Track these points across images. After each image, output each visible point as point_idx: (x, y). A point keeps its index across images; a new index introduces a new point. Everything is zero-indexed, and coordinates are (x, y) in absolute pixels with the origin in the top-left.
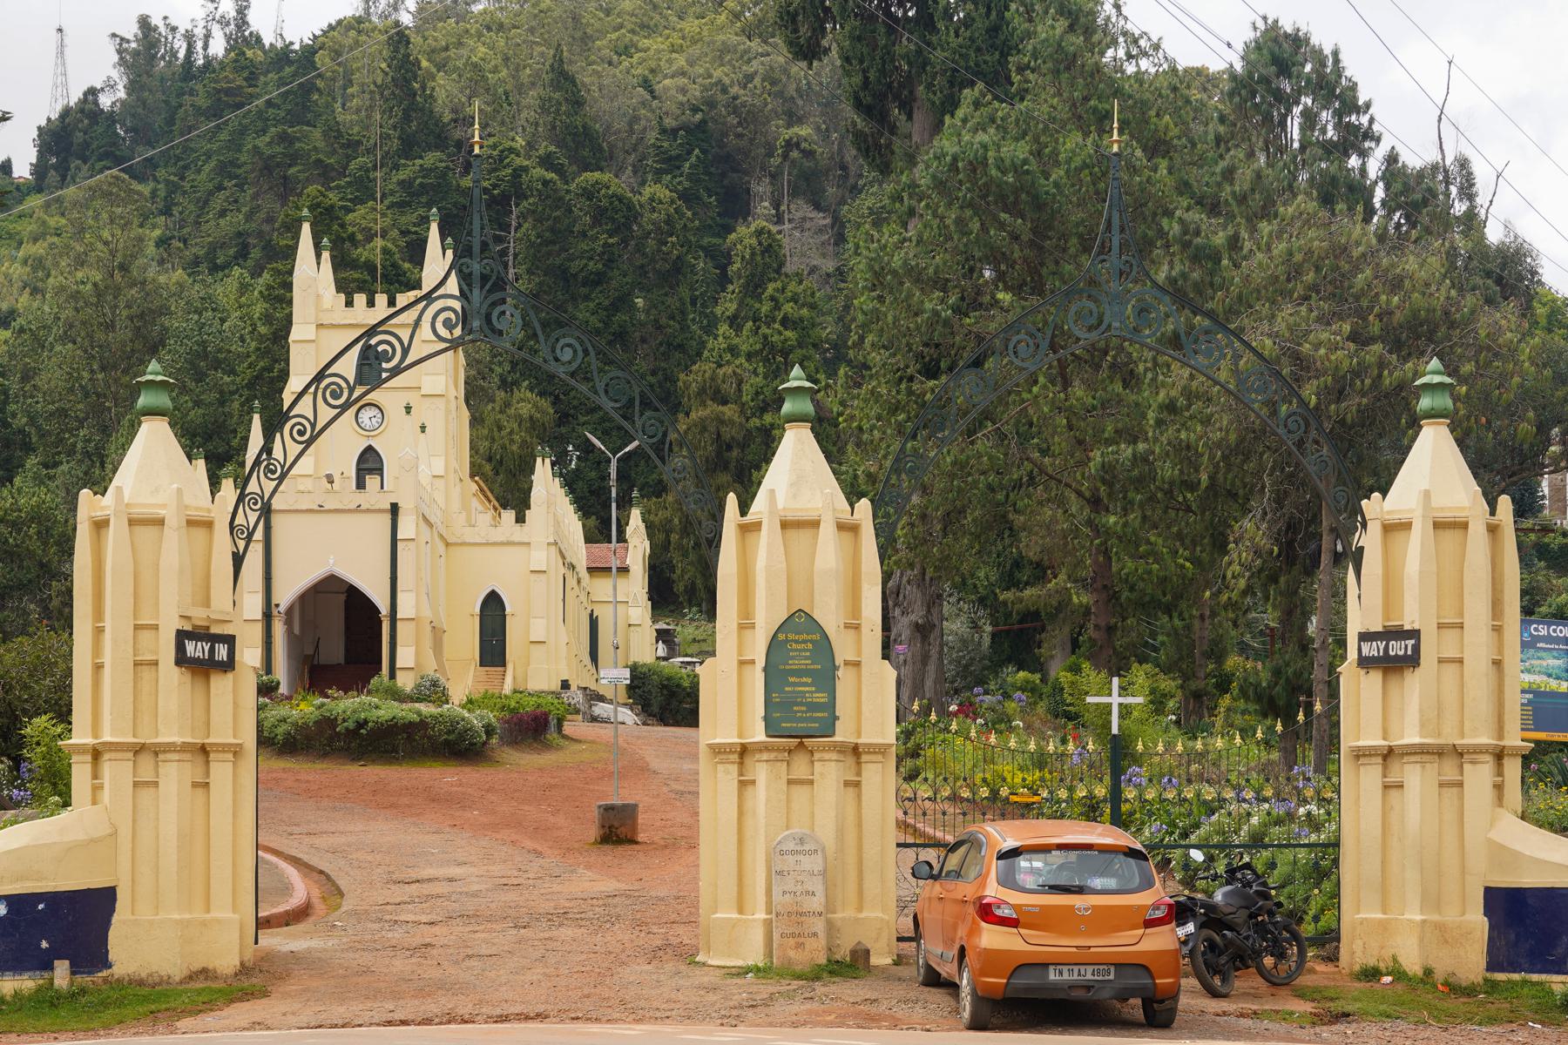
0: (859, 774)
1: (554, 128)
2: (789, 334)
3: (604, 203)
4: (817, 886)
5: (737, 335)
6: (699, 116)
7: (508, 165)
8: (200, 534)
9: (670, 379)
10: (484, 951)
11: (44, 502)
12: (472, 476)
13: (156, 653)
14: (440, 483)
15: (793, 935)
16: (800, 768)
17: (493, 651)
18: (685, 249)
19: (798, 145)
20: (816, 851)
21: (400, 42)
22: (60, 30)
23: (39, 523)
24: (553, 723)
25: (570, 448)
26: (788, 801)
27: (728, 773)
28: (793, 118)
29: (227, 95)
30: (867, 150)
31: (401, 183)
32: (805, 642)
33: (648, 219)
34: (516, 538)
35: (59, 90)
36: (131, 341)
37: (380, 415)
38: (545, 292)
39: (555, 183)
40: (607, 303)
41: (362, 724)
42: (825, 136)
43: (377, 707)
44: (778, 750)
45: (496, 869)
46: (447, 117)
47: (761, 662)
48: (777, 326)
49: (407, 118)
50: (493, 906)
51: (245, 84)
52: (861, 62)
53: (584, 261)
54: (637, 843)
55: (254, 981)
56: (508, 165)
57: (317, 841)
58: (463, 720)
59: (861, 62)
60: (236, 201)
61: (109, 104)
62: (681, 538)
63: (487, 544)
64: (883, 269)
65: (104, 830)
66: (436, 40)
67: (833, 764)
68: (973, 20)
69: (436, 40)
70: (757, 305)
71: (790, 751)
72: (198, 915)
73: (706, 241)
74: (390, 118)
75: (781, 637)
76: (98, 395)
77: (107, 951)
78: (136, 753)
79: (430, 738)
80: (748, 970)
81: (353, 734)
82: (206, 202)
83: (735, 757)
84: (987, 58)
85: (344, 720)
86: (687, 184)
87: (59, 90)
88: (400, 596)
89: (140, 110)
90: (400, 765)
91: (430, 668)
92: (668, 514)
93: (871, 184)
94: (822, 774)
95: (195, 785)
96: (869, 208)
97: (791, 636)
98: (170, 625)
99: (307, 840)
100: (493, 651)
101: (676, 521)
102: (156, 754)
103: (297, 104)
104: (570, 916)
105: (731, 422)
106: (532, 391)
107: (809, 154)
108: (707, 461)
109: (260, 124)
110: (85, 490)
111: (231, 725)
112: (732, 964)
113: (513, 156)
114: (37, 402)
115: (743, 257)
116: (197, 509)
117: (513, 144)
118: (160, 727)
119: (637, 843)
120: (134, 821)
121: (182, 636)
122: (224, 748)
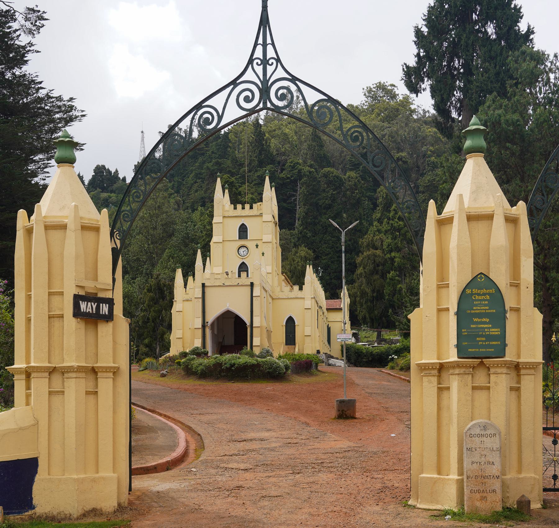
0: (519, 382)
1: (313, 155)
2: (401, 223)
3: (332, 179)
4: (496, 458)
5: (380, 226)
6: (365, 150)
7: (297, 169)
8: (91, 235)
9: (356, 242)
10: (273, 493)
11: (130, 290)
12: (282, 273)
13: (62, 309)
14: (270, 276)
15: (479, 491)
16: (481, 378)
17: (290, 339)
18: (361, 195)
19: (401, 159)
20: (495, 435)
21: (258, 126)
22: (142, 132)
23: (128, 298)
24: (314, 365)
25: (319, 268)
26: (473, 401)
27: (430, 382)
28: (399, 150)
29: (198, 151)
30: (442, 129)
31: (258, 176)
32: (484, 294)
33: (348, 184)
34: (299, 296)
35: (142, 152)
36: (162, 233)
37: (247, 250)
38: (310, 212)
39: (314, 173)
40: (332, 215)
41: (233, 365)
42: (411, 156)
43: (239, 358)
44: (466, 367)
45: (286, 433)
46: (275, 153)
47: (454, 308)
48: (396, 220)
49: (260, 154)
50: (282, 458)
51: (205, 146)
52: (440, 91)
53: (324, 200)
54: (355, 418)
55: (126, 516)
56: (297, 169)
57: (203, 418)
58: (276, 363)
59: (440, 91)
60: (201, 187)
61: (158, 156)
62: (361, 299)
63: (288, 299)
64: (454, 171)
65: (29, 422)
66: (271, 128)
67: (504, 376)
68: (489, 70)
69: (271, 128)
70: (388, 214)
71: (474, 368)
72: (91, 475)
73: (368, 194)
74: (254, 154)
75: (468, 291)
76: (150, 253)
77: (32, 499)
78: (50, 373)
79: (261, 371)
80: (446, 513)
81: (229, 369)
82: (191, 188)
83: (435, 372)
84: (495, 85)
85: (225, 364)
86: (361, 174)
87: (142, 152)
88: (254, 318)
89: (169, 158)
90: (249, 382)
91: (266, 345)
92: (356, 290)
93: (429, 171)
94: (496, 383)
95: (88, 393)
96: (428, 180)
97: (475, 291)
98: (70, 291)
99: (199, 417)
100: (290, 339)
101: (359, 293)
102: (63, 373)
103: (222, 152)
104: (325, 465)
105: (379, 256)
106: (305, 247)
107: (405, 162)
108: (370, 270)
109: (209, 159)
110: (21, 210)
111: (111, 353)
112: (434, 508)
113: (298, 165)
114: (130, 256)
115: (383, 197)
116: (89, 219)
117: (298, 161)
118: (65, 357)
119: (355, 418)
120: (49, 416)
121: (77, 299)
122: (107, 369)
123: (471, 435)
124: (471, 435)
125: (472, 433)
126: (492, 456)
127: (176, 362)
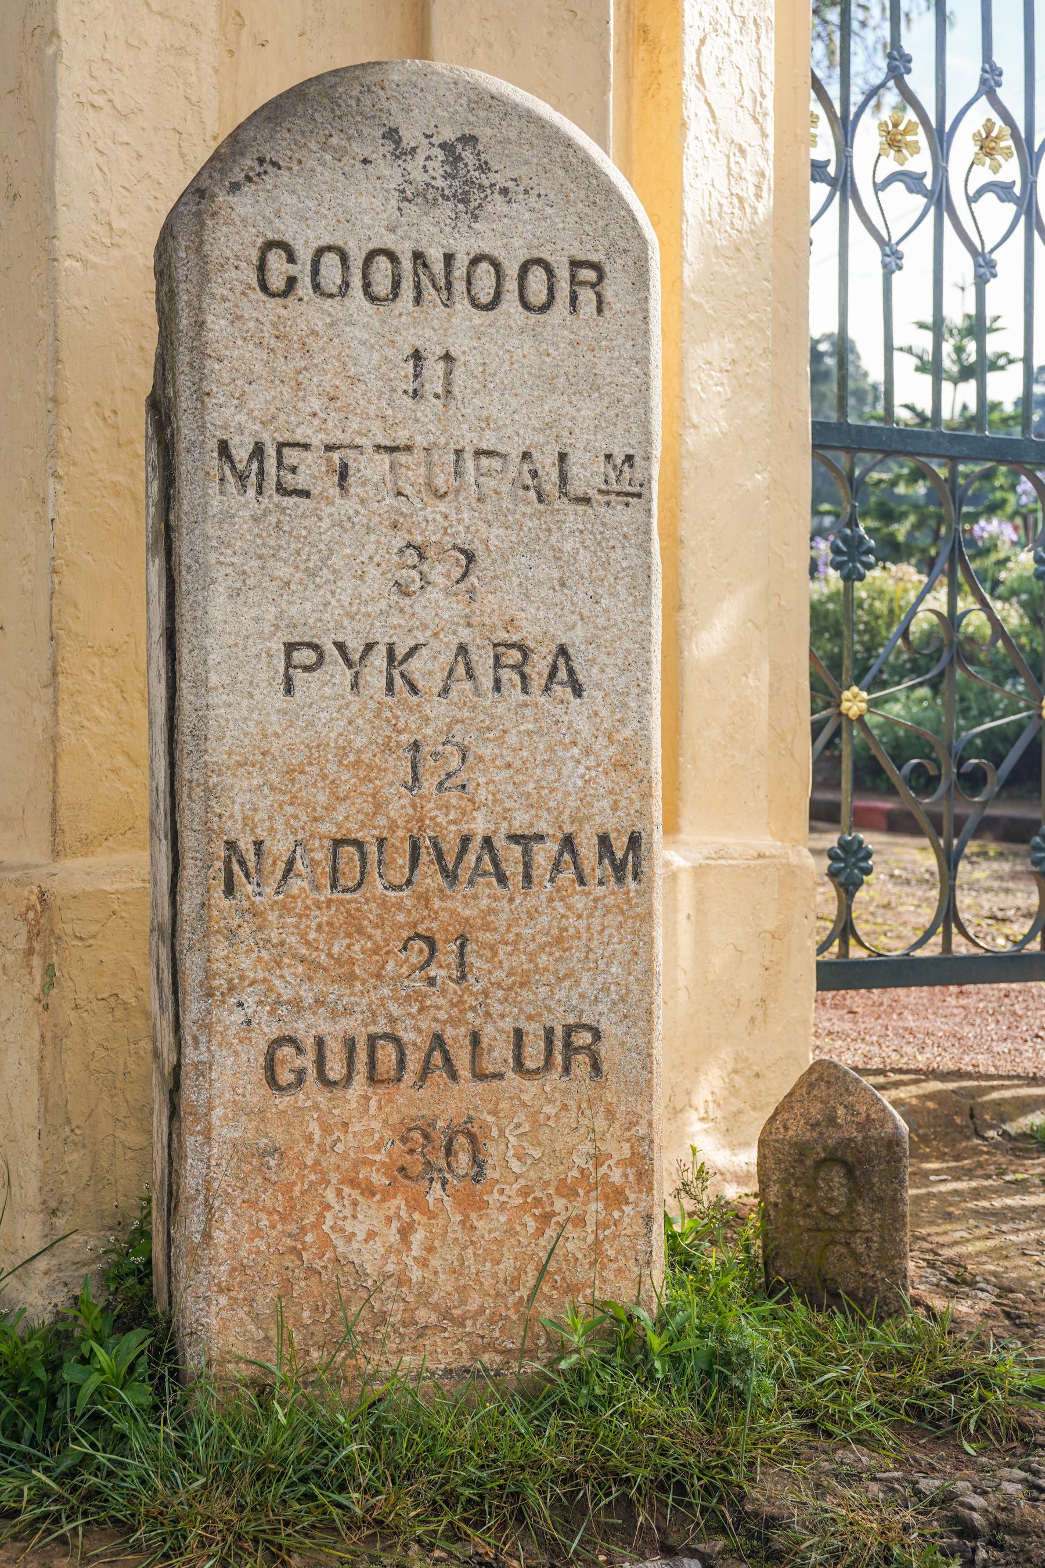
123: (276, 261)
124: (276, 261)
125: (288, 230)
126: (547, 571)
127: (912, 519)
